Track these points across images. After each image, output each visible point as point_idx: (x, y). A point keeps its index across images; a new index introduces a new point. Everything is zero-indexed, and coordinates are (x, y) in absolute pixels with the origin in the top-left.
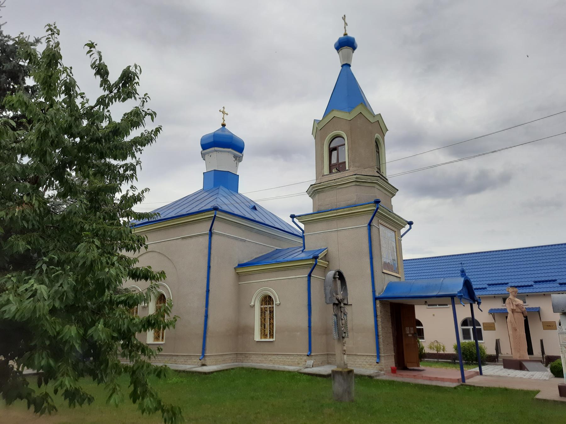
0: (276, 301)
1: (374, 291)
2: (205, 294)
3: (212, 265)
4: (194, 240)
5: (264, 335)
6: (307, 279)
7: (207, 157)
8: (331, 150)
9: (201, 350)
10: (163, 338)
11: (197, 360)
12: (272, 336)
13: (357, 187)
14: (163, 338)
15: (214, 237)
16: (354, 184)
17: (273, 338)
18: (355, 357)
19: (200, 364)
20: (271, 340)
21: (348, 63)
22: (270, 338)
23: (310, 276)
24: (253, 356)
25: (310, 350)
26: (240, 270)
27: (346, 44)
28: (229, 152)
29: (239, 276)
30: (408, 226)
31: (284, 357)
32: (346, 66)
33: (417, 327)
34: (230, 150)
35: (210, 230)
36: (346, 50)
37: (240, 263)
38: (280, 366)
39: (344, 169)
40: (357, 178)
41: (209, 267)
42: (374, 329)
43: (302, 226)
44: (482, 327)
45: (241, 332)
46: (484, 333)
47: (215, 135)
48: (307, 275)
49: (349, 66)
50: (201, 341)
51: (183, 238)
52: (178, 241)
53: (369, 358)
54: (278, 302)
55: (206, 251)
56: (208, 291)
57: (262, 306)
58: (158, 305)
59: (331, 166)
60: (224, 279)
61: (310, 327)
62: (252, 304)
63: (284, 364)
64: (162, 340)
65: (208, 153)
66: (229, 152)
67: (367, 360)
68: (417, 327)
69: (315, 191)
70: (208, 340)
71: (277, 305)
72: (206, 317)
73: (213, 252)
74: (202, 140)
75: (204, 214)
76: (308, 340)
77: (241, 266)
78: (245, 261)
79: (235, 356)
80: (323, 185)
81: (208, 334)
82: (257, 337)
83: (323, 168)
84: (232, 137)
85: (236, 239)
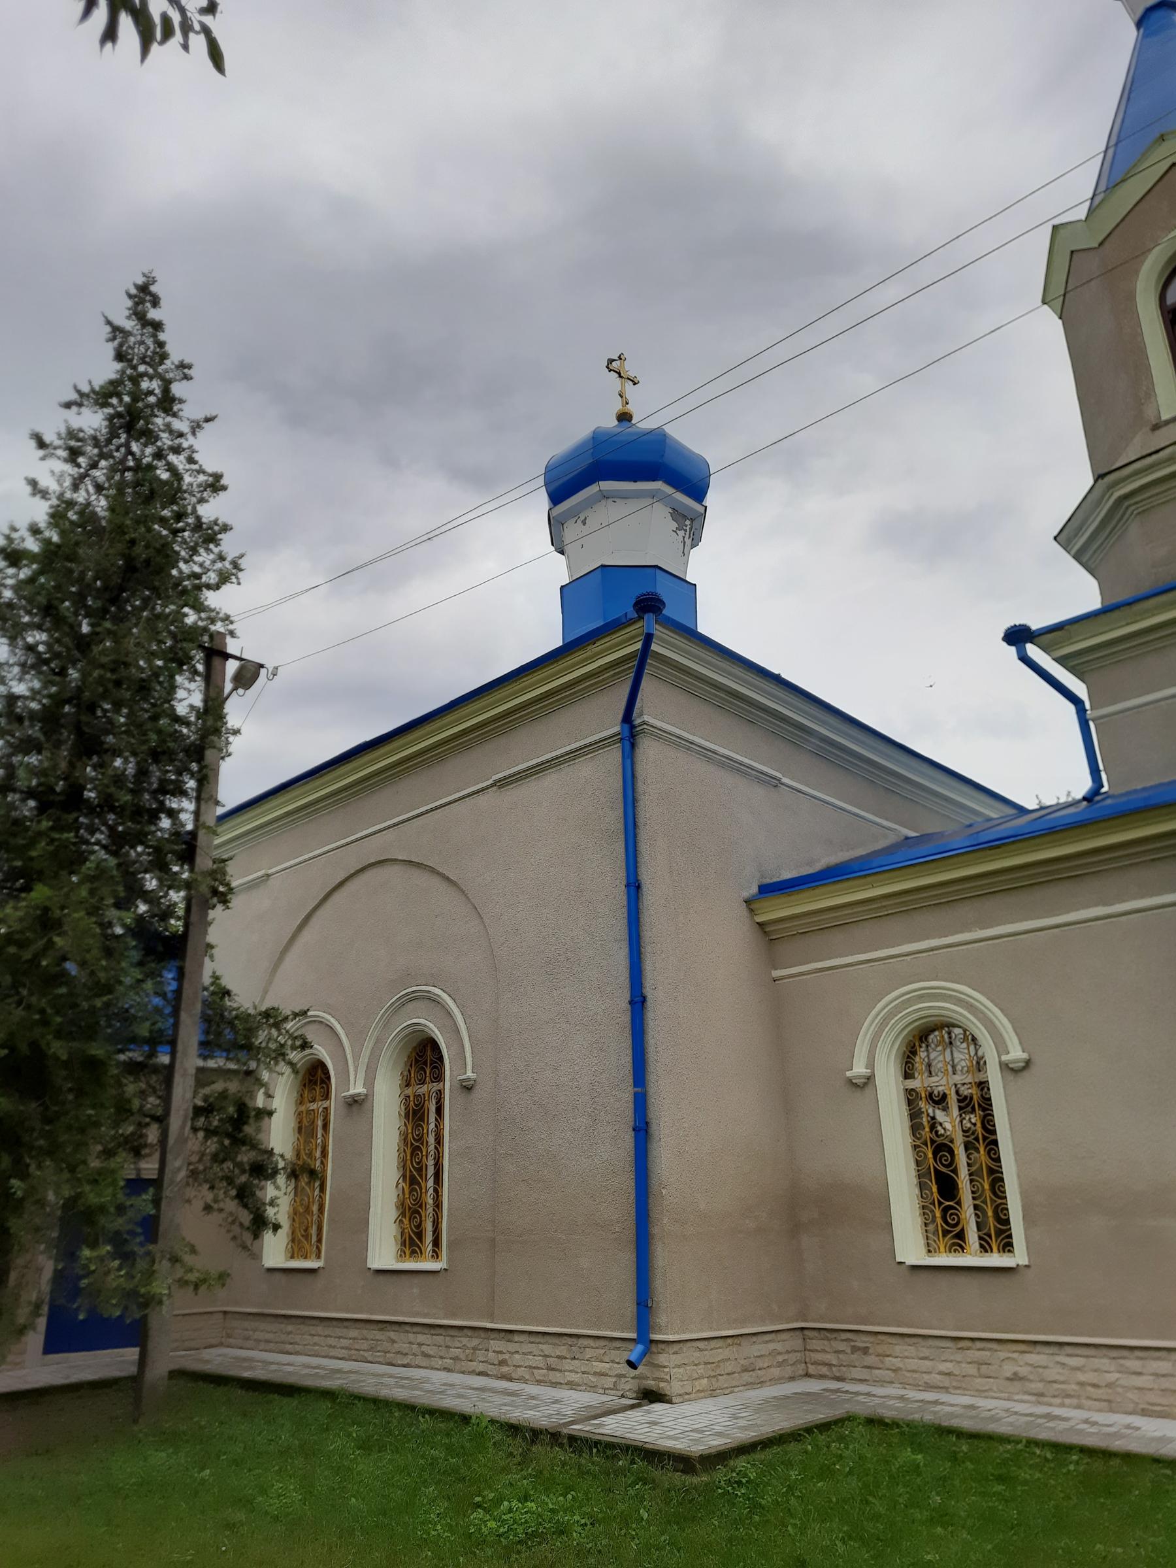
0: (1002, 1047)
2: (626, 1019)
3: (645, 877)
4: (551, 780)
7: (571, 531)
9: (630, 1308)
10: (436, 1243)
11: (612, 1363)
12: (998, 1235)
14: (436, 1243)
15: (649, 751)
17: (1007, 1246)
19: (630, 1385)
20: (996, 1260)
22: (985, 1248)
24: (900, 1348)
26: (777, 910)
28: (652, 495)
31: (1103, 1363)
35: (627, 718)
37: (768, 881)
38: (983, 1403)
41: (634, 887)
43: (1079, 688)
45: (813, 1214)
47: (598, 440)
50: (628, 1258)
51: (502, 784)
52: (481, 799)
54: (1016, 1053)
55: (614, 818)
56: (638, 1003)
58: (409, 1091)
60: (703, 949)
62: (859, 1069)
63: (1111, 1406)
64: (436, 1255)
65: (573, 514)
66: (652, 495)
70: (661, 1256)
72: (642, 1130)
74: (548, 470)
75: (593, 649)
77: (767, 890)
78: (787, 875)
79: (795, 1342)
81: (663, 1223)
82: (910, 1243)
84: (659, 439)
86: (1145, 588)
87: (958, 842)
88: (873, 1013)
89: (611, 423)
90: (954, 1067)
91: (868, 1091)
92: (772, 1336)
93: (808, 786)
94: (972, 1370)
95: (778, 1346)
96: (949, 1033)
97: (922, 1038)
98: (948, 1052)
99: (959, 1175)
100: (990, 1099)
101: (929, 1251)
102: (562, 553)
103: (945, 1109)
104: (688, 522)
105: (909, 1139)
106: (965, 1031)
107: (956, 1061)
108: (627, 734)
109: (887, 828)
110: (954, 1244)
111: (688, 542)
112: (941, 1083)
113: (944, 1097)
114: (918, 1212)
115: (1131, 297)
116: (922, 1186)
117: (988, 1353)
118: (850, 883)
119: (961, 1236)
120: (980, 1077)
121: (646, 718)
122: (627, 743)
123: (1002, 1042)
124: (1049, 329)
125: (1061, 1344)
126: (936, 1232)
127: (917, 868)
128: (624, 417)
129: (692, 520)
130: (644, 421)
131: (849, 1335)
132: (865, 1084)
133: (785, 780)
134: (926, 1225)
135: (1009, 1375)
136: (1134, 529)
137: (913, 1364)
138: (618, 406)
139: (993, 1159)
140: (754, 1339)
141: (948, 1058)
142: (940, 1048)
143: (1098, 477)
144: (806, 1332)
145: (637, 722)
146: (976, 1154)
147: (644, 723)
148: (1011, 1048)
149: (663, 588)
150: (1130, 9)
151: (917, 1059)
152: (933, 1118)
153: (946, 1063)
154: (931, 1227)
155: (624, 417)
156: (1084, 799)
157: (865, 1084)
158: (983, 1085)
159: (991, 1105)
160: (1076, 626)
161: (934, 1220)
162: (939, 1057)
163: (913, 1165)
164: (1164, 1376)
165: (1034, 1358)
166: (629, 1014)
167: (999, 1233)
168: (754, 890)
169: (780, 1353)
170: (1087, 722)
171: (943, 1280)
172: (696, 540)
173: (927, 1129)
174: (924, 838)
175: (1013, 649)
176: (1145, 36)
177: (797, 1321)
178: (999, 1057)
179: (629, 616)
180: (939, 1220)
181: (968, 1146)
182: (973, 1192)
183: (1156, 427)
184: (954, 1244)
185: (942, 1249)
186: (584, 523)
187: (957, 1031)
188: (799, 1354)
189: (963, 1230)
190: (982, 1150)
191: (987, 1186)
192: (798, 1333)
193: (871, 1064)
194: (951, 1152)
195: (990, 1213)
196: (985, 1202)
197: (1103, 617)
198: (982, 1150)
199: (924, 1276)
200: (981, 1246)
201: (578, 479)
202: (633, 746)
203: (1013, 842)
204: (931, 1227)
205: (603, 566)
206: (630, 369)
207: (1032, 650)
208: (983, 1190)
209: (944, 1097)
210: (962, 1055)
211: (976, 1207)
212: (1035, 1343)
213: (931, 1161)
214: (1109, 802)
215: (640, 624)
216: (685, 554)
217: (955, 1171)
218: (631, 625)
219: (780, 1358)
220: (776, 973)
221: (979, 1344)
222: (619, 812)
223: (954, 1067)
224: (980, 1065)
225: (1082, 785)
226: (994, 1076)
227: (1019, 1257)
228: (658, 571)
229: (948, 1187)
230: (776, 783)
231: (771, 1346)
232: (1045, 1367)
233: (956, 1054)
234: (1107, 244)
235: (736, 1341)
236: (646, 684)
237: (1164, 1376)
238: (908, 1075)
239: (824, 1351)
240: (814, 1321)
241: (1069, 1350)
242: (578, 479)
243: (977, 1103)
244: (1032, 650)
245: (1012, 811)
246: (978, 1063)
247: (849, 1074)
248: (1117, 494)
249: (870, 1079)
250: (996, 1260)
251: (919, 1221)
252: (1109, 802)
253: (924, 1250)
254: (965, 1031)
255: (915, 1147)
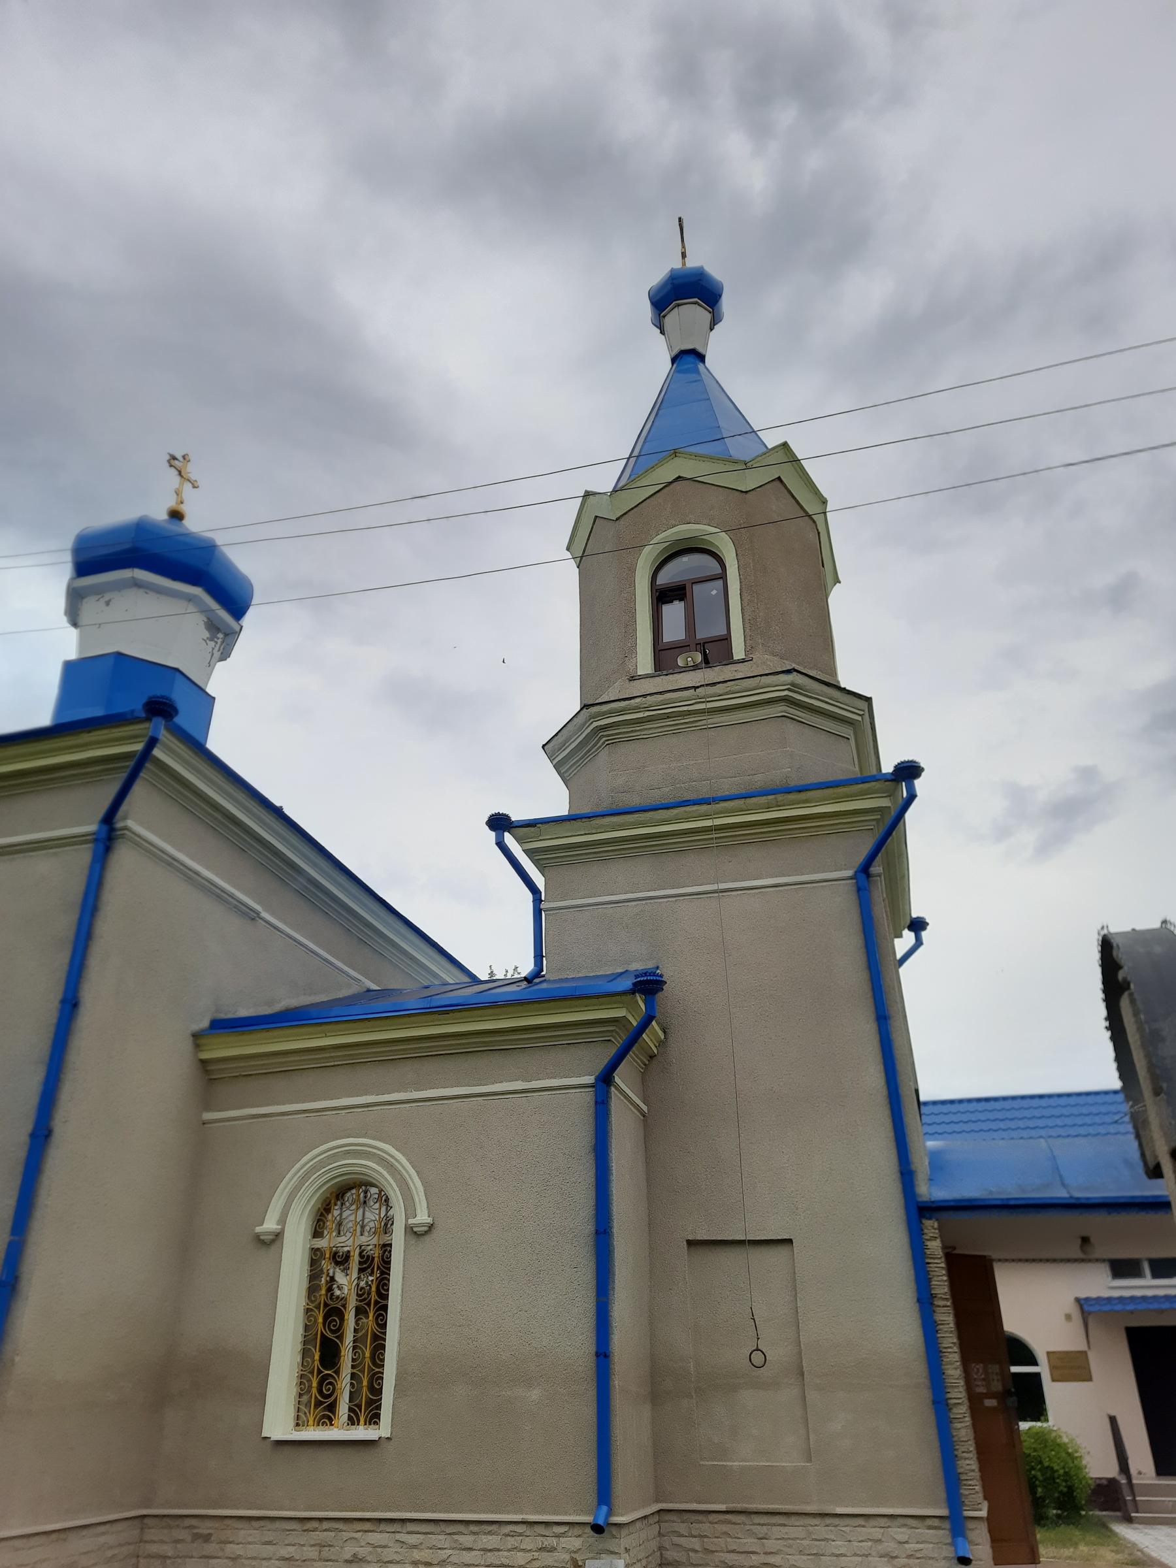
0: (410, 1211)
1: (907, 1175)
2: (21, 1154)
5: (319, 1401)
6: (588, 1097)
7: (91, 608)
8: (663, 596)
13: (791, 727)
15: (124, 859)
16: (779, 709)
17: (374, 1418)
18: (821, 1529)
20: (361, 1433)
21: (700, 350)
22: (353, 1421)
23: (605, 1079)
24: (246, 1533)
25: (604, 1494)
27: (687, 293)
29: (211, 1077)
30: (908, 937)
31: (439, 1540)
32: (688, 358)
33: (1015, 1369)
34: (197, 591)
36: (691, 313)
37: (222, 1016)
39: (727, 658)
40: (794, 687)
41: (70, 1005)
42: (920, 1369)
44: (1043, 1369)
46: (1054, 1393)
47: (141, 528)
48: (590, 1079)
49: (702, 358)
53: (899, 1532)
54: (422, 1217)
55: (65, 924)
57: (321, 1243)
59: (664, 657)
61: (603, 1355)
62: (270, 1225)
65: (98, 590)
66: (190, 599)
67: (890, 1546)
68: (1015, 1369)
69: (570, 751)
71: (415, 1234)
73: (107, 927)
75: (85, 738)
76: (591, 1435)
77: (221, 1026)
78: (243, 1013)
80: (637, 709)
82: (279, 1421)
83: (633, 649)
84: (208, 549)
85: (221, 896)
86: (604, 807)
87: (412, 1003)
88: (298, 1166)
89: (159, 514)
90: (363, 1227)
91: (274, 1248)
92: (107, 1527)
93: (285, 923)
94: (312, 1553)
95: (110, 1539)
96: (366, 1192)
97: (345, 1192)
98: (360, 1212)
99: (342, 1344)
100: (389, 1263)
101: (298, 1425)
102: (75, 624)
103: (346, 1270)
104: (220, 635)
105: (303, 1302)
106: (381, 1191)
107: (366, 1221)
108: (103, 835)
109: (352, 977)
110: (324, 1416)
111: (217, 655)
112: (348, 1242)
113: (347, 1257)
114: (295, 1381)
115: (632, 570)
116: (305, 1353)
117: (333, 1534)
118: (311, 1029)
119: (332, 1408)
120: (385, 1239)
121: (130, 823)
122: (101, 847)
123: (412, 1205)
124: (570, 573)
125: (403, 1521)
126: (308, 1405)
127: (372, 1023)
128: (176, 515)
129: (226, 635)
130: (196, 523)
131: (194, 1522)
132: (273, 1241)
133: (264, 915)
134: (300, 1395)
135: (348, 1556)
136: (603, 757)
137: (253, 1550)
138: (171, 503)
139: (378, 1324)
140: (85, 1532)
141: (359, 1218)
142: (354, 1207)
143: (585, 707)
144: (146, 1521)
145: (119, 825)
146: (364, 1320)
147: (126, 828)
148: (418, 1211)
149: (179, 696)
150: (670, 348)
151: (330, 1217)
152: (332, 1279)
153: (356, 1223)
154: (305, 1398)
155: (176, 515)
156: (525, 979)
157: (273, 1241)
158: (386, 1248)
159: (389, 1269)
160: (546, 826)
161: (309, 1391)
162: (350, 1215)
163: (301, 1330)
164: (490, 1550)
165: (376, 1538)
166: (26, 1148)
167: (370, 1403)
168: (205, 1024)
169: (111, 1548)
170: (540, 911)
171: (306, 1454)
172: (225, 655)
173: (323, 1292)
174: (385, 993)
175: (493, 834)
176: (677, 371)
177: (139, 1508)
178: (407, 1220)
179: (136, 714)
180: (314, 1391)
181: (360, 1312)
182: (353, 1360)
183: (632, 679)
184: (324, 1416)
185: (311, 1422)
186: (108, 603)
187: (373, 1190)
188: (132, 1547)
189: (336, 1399)
190: (371, 1318)
191: (367, 1354)
192: (136, 1522)
193: (283, 1221)
194: (342, 1318)
195: (365, 1383)
196: (363, 1371)
197: (567, 824)
198: (371, 1318)
199: (287, 1450)
200: (350, 1418)
201: (109, 559)
202: (108, 849)
203: (460, 1011)
204: (305, 1398)
205: (119, 655)
206: (192, 471)
207: (509, 839)
208: (364, 1358)
209: (347, 1257)
210: (372, 1215)
211: (353, 1376)
212: (380, 1520)
213: (320, 1326)
214: (544, 986)
215: (146, 725)
216: (210, 666)
217: (341, 1338)
218: (131, 726)
219: (109, 1553)
220: (208, 1116)
221: (326, 1525)
222: (74, 917)
223: (363, 1227)
224: (387, 1226)
225: (527, 967)
226: (398, 1239)
227: (384, 1429)
228: (178, 674)
229: (329, 1354)
230: (252, 916)
231: (102, 1540)
232: (385, 1547)
233: (368, 1214)
234: (622, 521)
235: (63, 1536)
236: (139, 790)
237: (490, 1550)
238: (317, 1234)
239: (162, 1542)
240: (163, 1506)
241: (411, 1527)
242: (109, 559)
243: (377, 1265)
244: (509, 839)
245: (467, 980)
246: (386, 1225)
247: (258, 1229)
248: (595, 724)
249: (278, 1236)
250: (361, 1433)
251: (294, 1391)
252: (544, 986)
253: (292, 1423)
254: (381, 1191)
255: (308, 1310)
